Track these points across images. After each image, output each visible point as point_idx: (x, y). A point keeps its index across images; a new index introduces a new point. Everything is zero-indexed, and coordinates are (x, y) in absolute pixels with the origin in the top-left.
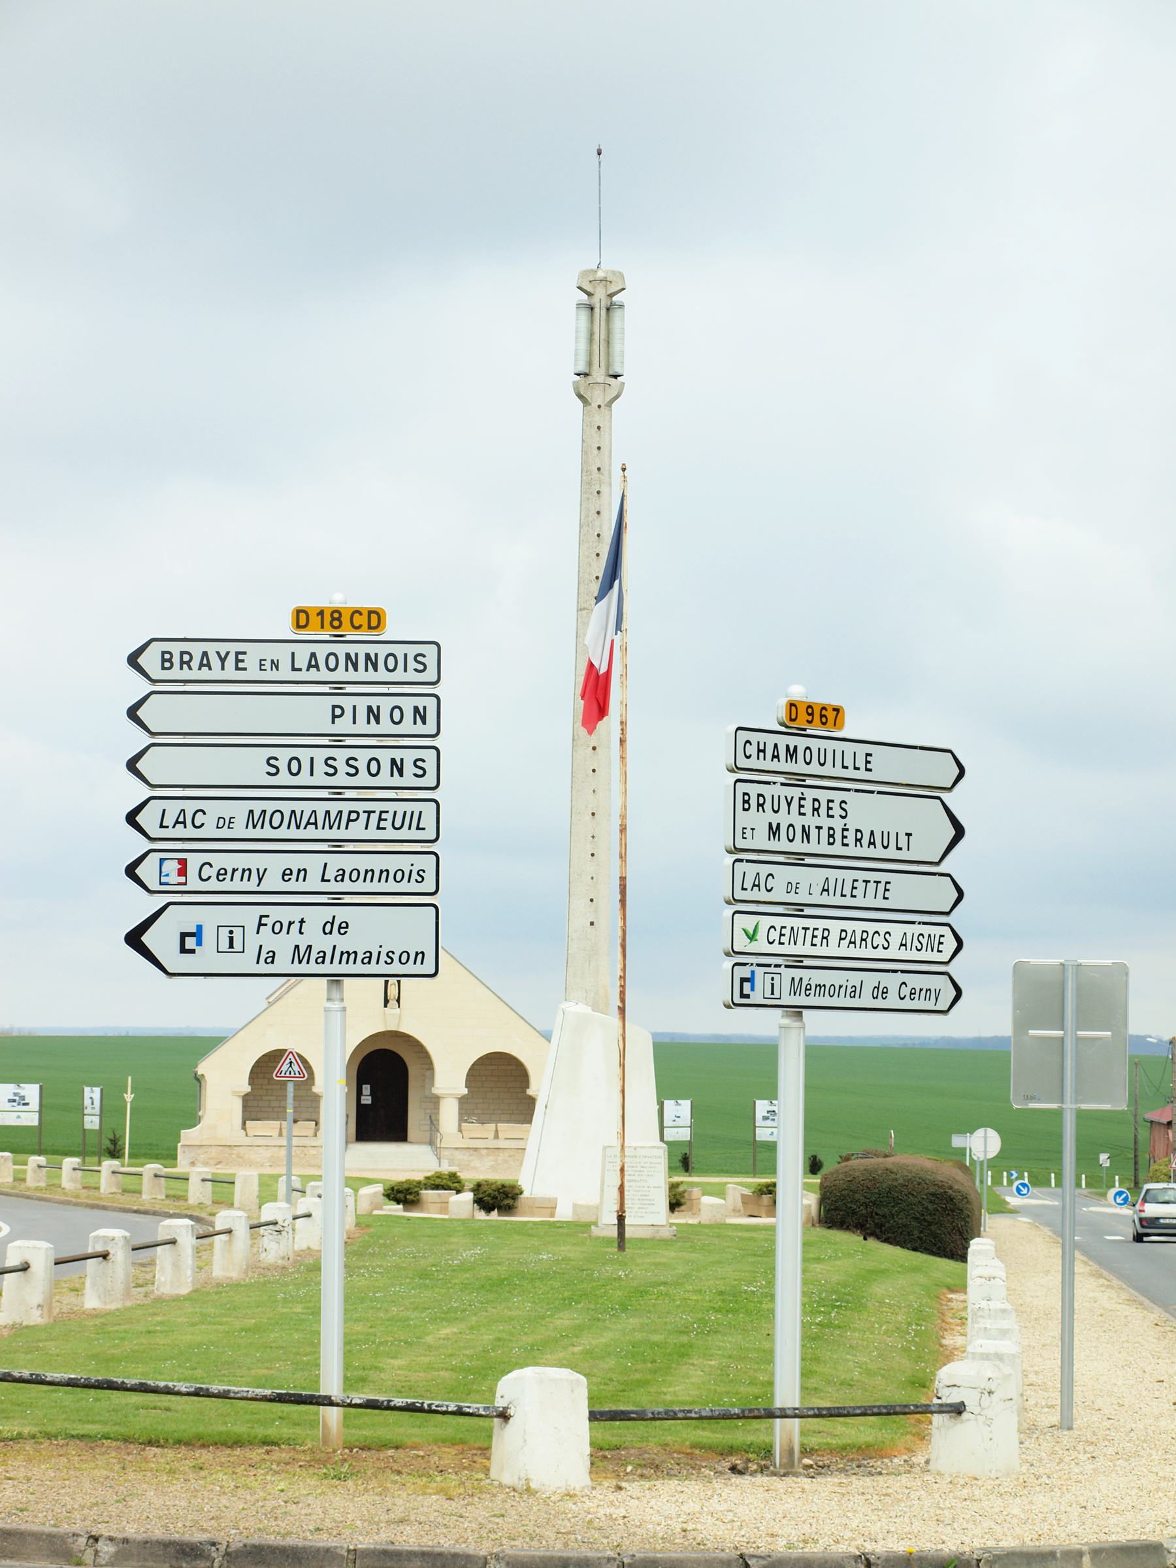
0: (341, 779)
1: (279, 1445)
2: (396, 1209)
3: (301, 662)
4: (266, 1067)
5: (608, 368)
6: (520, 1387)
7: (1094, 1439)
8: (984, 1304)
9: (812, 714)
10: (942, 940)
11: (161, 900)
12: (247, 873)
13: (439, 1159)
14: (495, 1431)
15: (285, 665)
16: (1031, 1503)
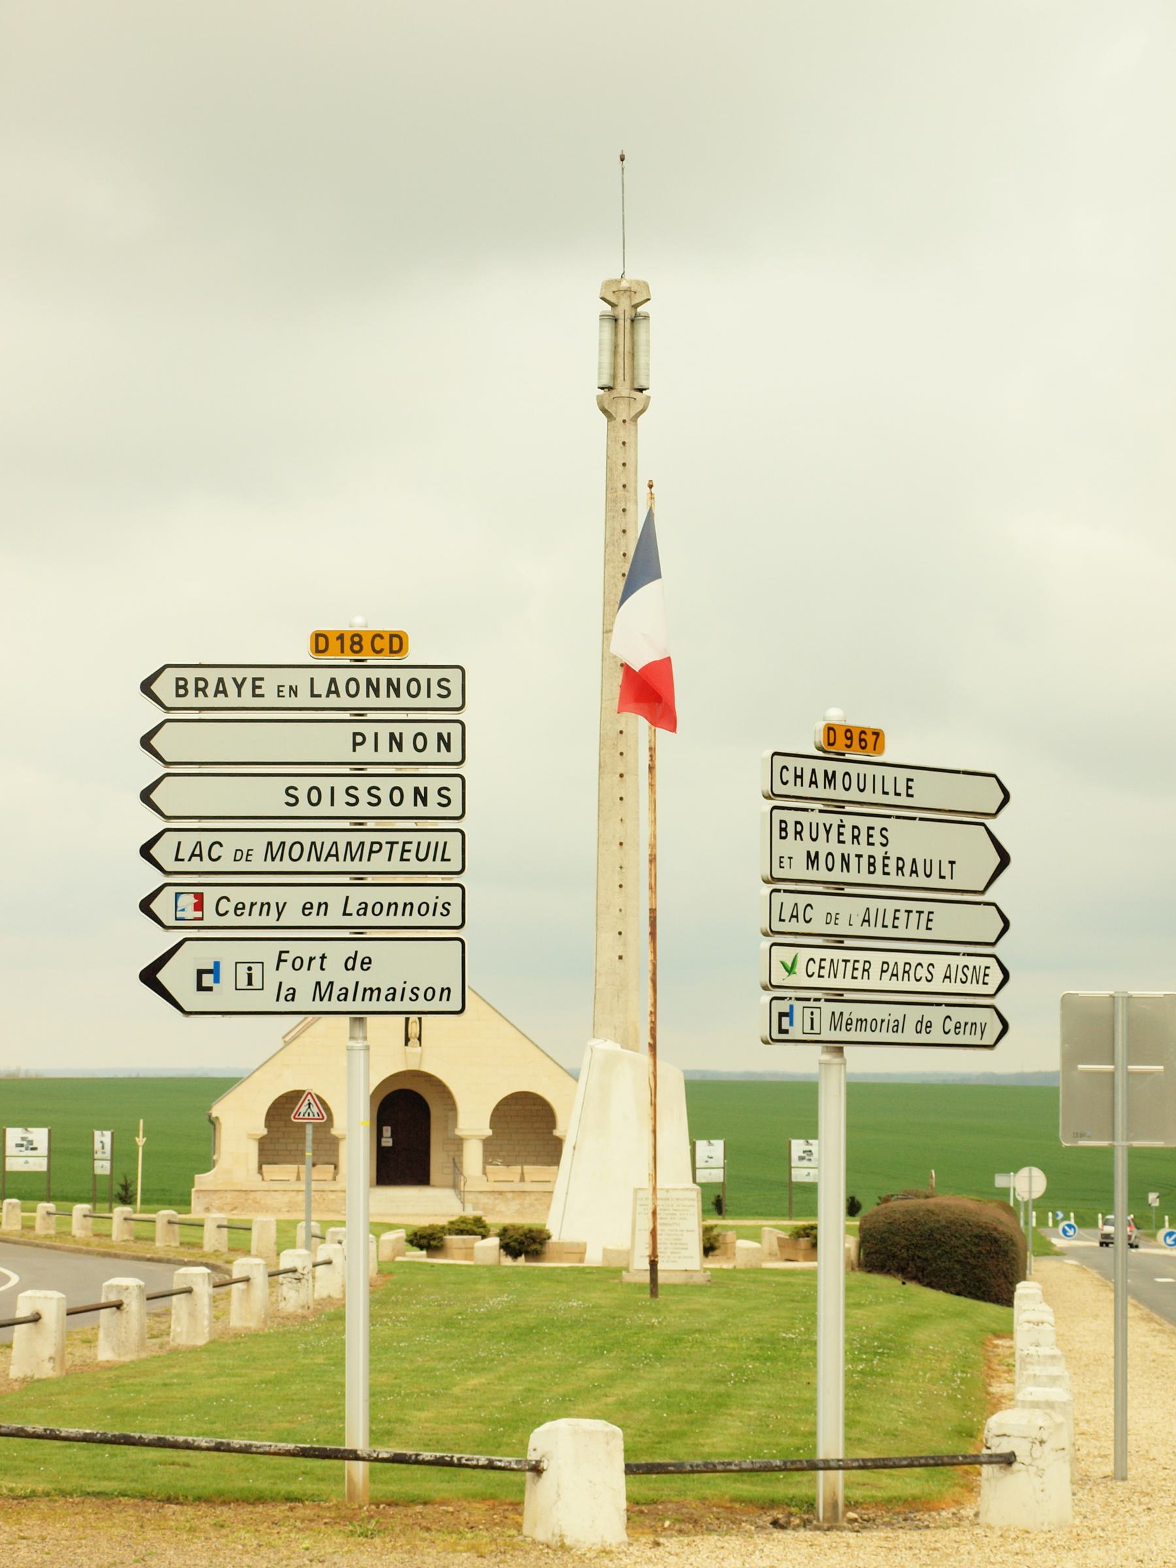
0: (362, 809)
1: (302, 1502)
2: (419, 1255)
3: (321, 687)
4: (283, 1109)
5: (632, 383)
6: (553, 1439)
7: (1149, 1490)
8: (1032, 1350)
9: (851, 738)
10: (988, 971)
11: (177, 936)
12: (266, 907)
13: (463, 1203)
14: (528, 1486)
15: (304, 691)
16: (1086, 1557)
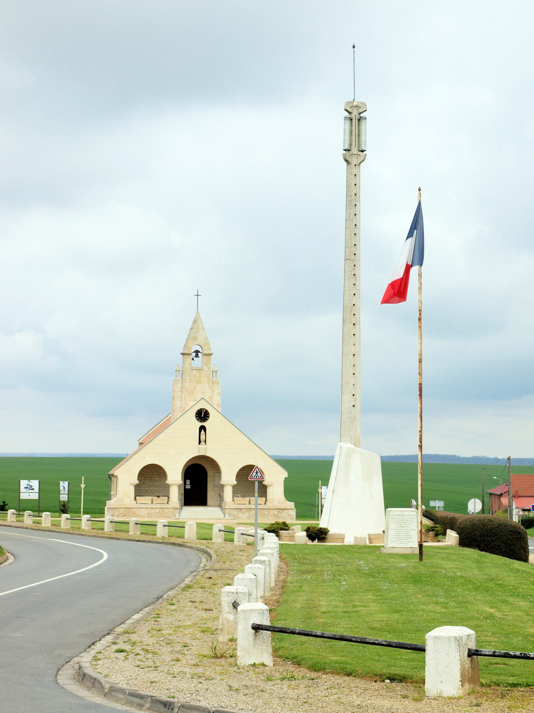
13: (224, 514)
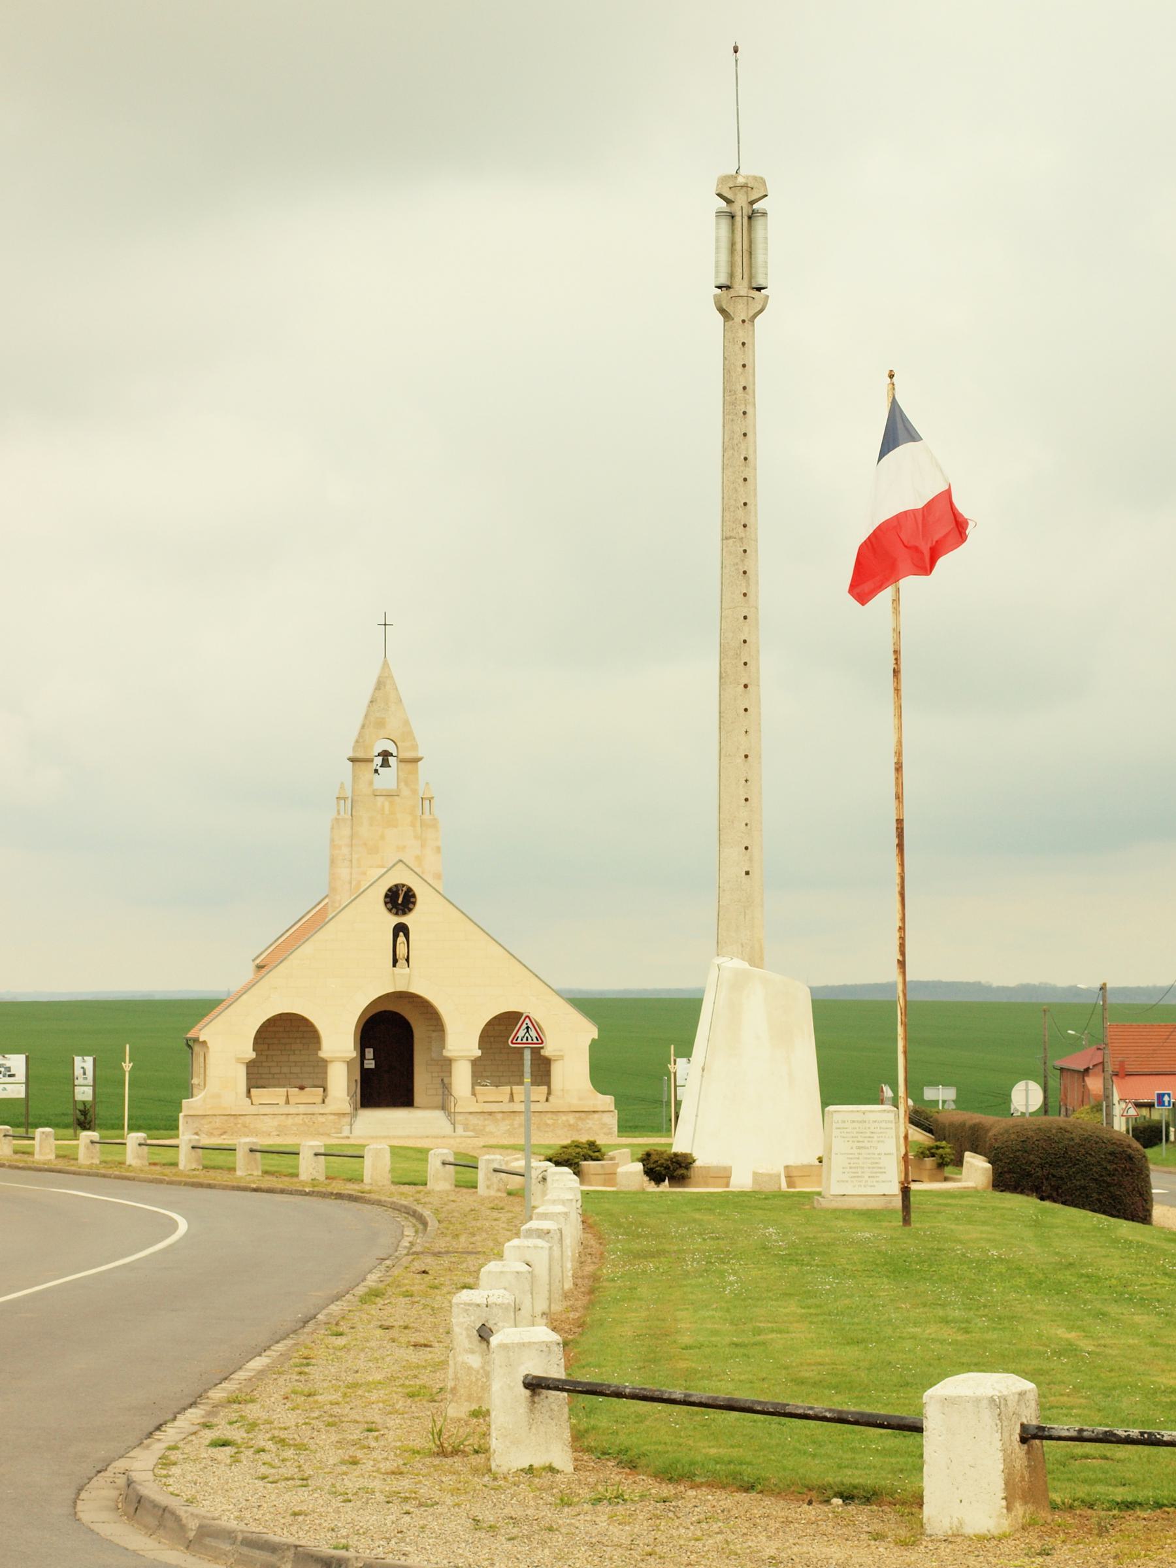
5: (750, 282)
13: (454, 1124)
